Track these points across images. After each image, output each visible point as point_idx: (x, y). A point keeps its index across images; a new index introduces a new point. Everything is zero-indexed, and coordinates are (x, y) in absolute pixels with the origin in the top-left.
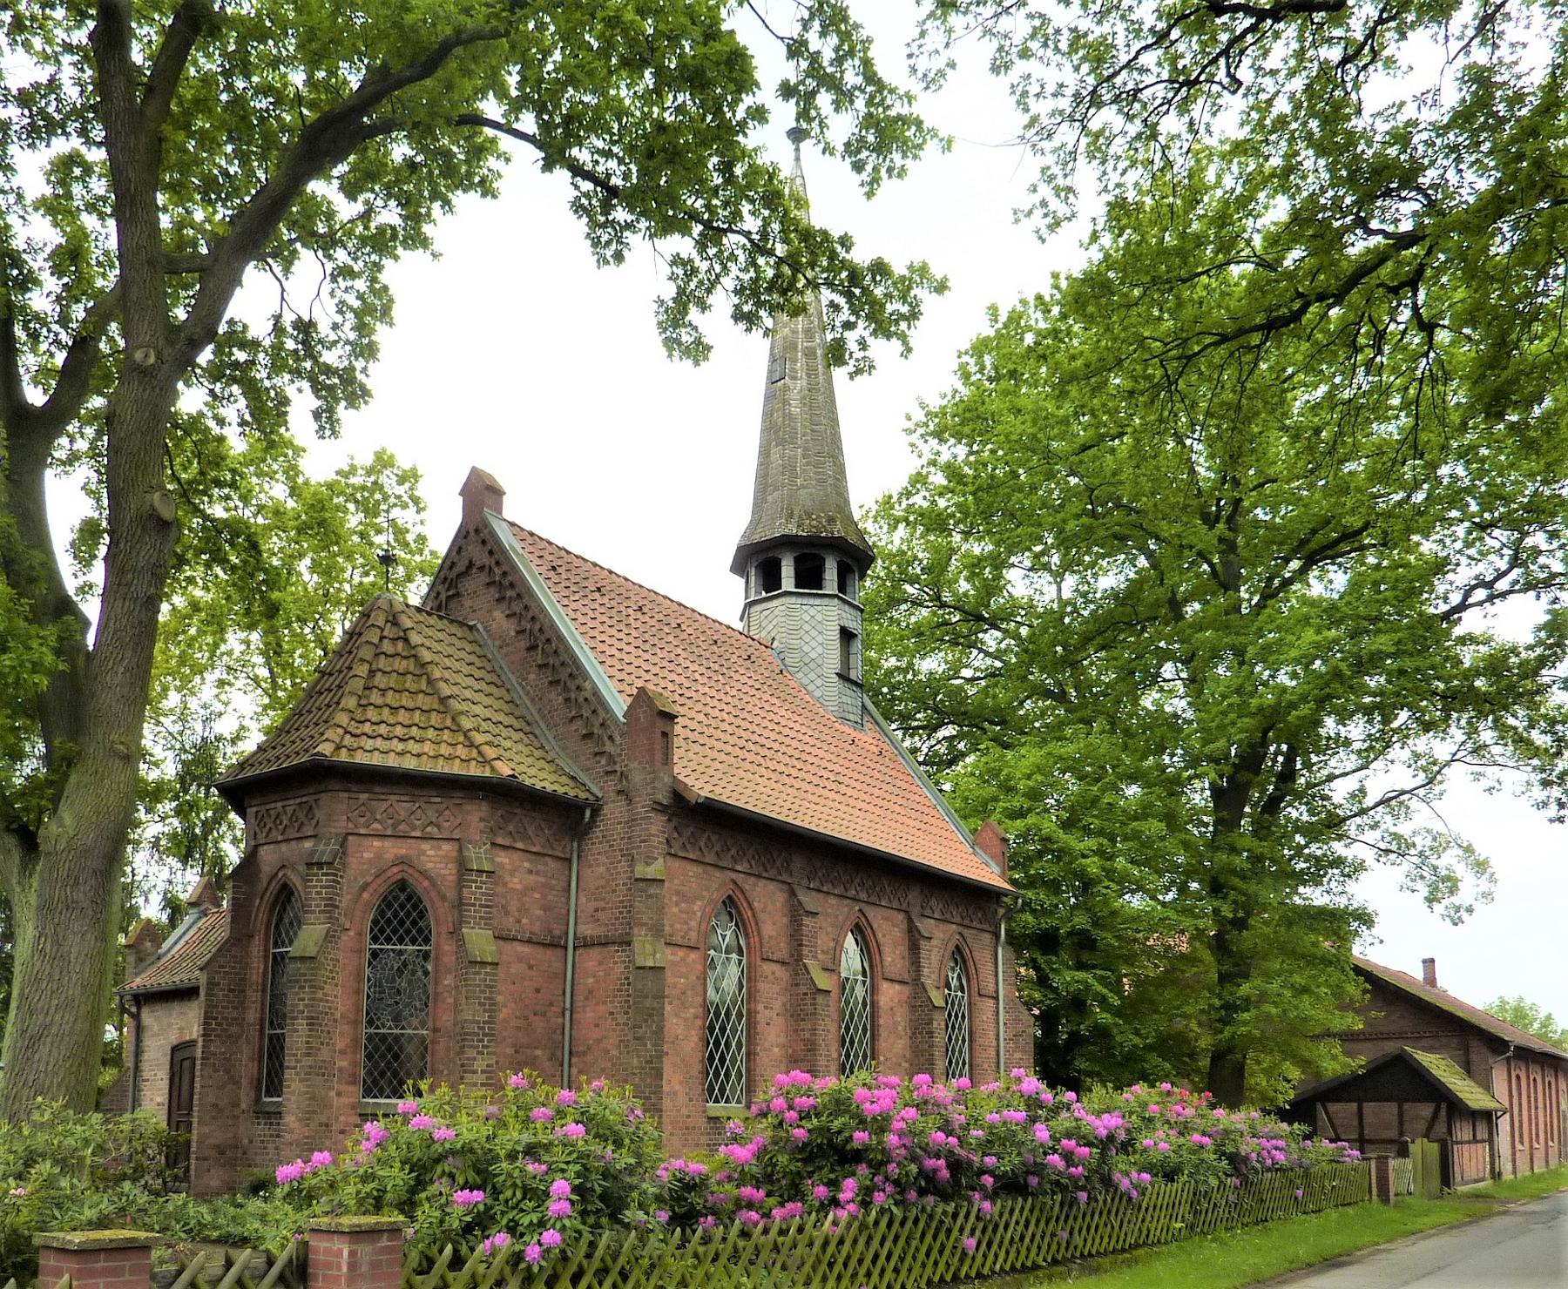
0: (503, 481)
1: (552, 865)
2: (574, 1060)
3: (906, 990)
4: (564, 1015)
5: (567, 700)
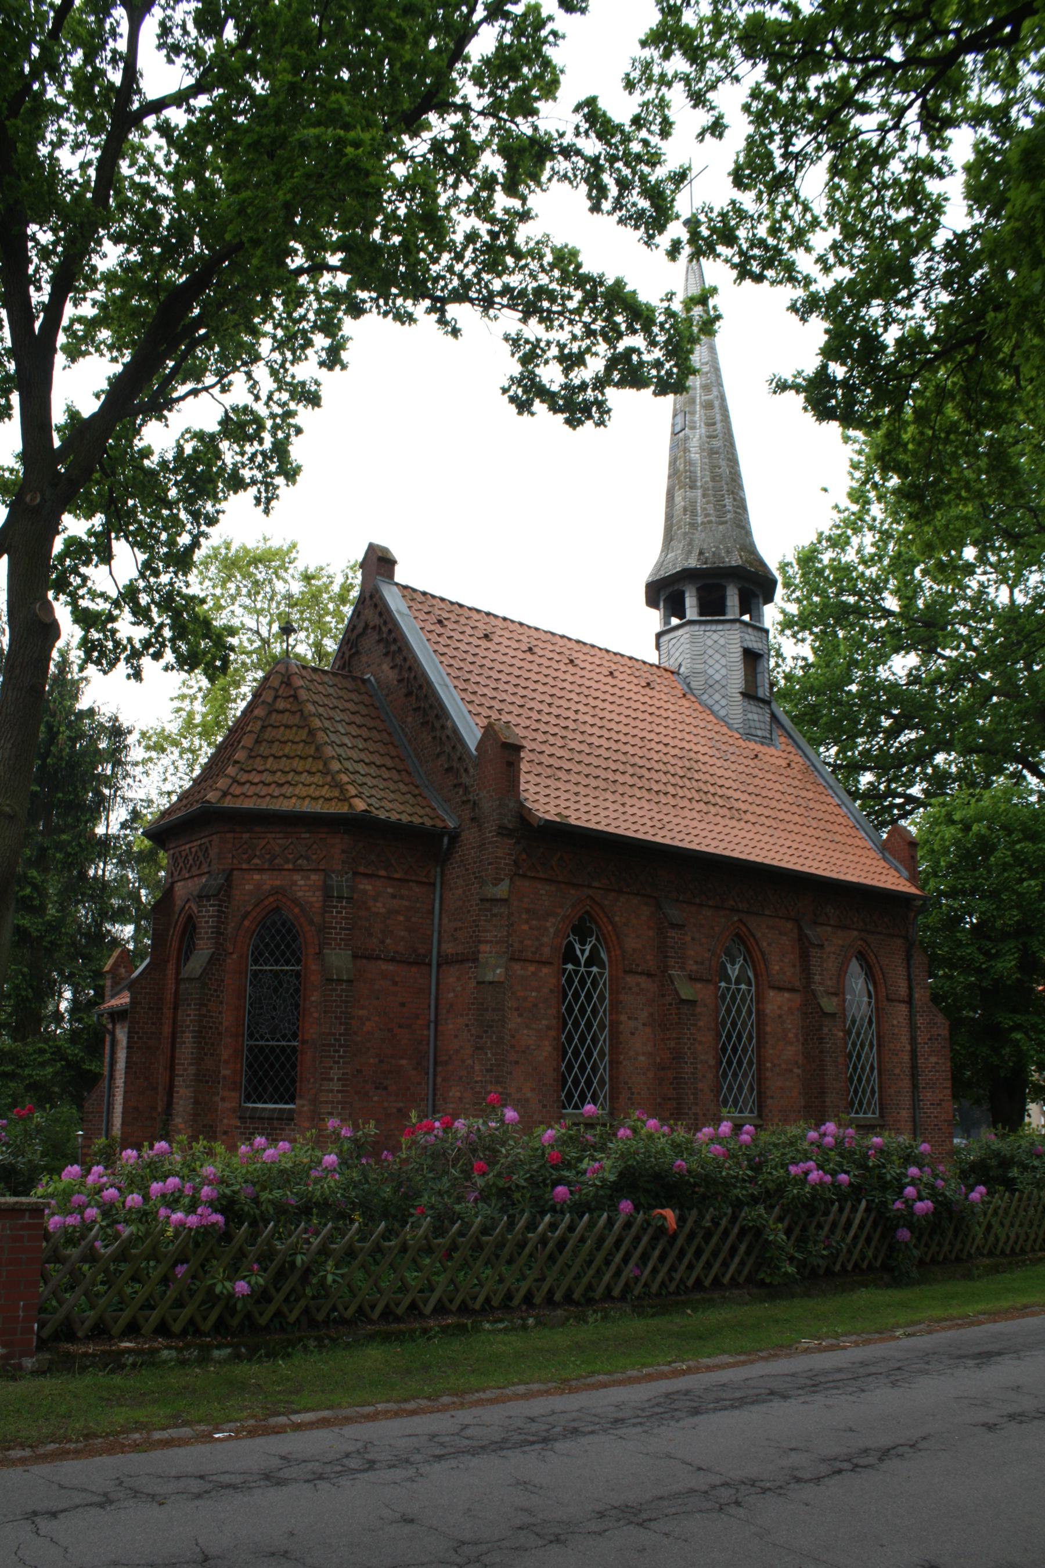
0: (396, 553)
1: (789, 925)
2: (439, 1069)
3: (798, 998)
4: (429, 1028)
5: (434, 738)
